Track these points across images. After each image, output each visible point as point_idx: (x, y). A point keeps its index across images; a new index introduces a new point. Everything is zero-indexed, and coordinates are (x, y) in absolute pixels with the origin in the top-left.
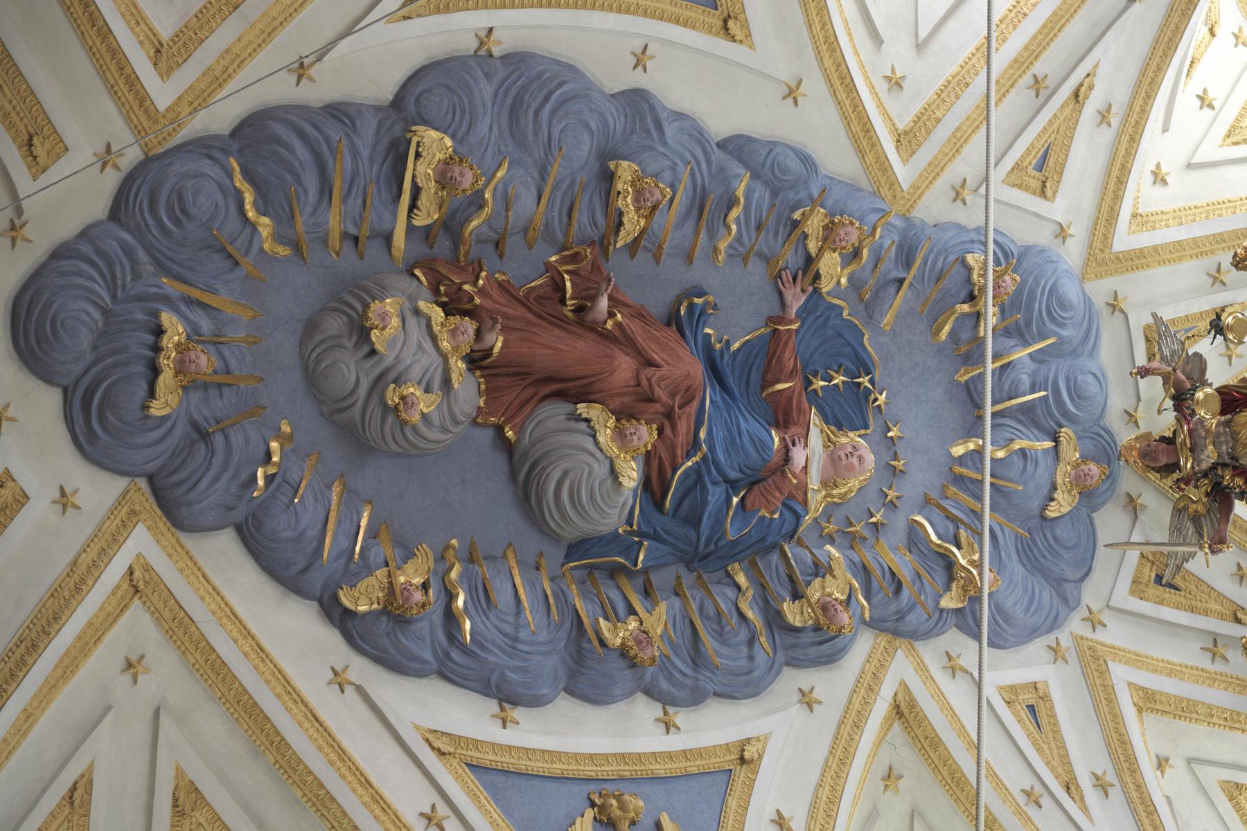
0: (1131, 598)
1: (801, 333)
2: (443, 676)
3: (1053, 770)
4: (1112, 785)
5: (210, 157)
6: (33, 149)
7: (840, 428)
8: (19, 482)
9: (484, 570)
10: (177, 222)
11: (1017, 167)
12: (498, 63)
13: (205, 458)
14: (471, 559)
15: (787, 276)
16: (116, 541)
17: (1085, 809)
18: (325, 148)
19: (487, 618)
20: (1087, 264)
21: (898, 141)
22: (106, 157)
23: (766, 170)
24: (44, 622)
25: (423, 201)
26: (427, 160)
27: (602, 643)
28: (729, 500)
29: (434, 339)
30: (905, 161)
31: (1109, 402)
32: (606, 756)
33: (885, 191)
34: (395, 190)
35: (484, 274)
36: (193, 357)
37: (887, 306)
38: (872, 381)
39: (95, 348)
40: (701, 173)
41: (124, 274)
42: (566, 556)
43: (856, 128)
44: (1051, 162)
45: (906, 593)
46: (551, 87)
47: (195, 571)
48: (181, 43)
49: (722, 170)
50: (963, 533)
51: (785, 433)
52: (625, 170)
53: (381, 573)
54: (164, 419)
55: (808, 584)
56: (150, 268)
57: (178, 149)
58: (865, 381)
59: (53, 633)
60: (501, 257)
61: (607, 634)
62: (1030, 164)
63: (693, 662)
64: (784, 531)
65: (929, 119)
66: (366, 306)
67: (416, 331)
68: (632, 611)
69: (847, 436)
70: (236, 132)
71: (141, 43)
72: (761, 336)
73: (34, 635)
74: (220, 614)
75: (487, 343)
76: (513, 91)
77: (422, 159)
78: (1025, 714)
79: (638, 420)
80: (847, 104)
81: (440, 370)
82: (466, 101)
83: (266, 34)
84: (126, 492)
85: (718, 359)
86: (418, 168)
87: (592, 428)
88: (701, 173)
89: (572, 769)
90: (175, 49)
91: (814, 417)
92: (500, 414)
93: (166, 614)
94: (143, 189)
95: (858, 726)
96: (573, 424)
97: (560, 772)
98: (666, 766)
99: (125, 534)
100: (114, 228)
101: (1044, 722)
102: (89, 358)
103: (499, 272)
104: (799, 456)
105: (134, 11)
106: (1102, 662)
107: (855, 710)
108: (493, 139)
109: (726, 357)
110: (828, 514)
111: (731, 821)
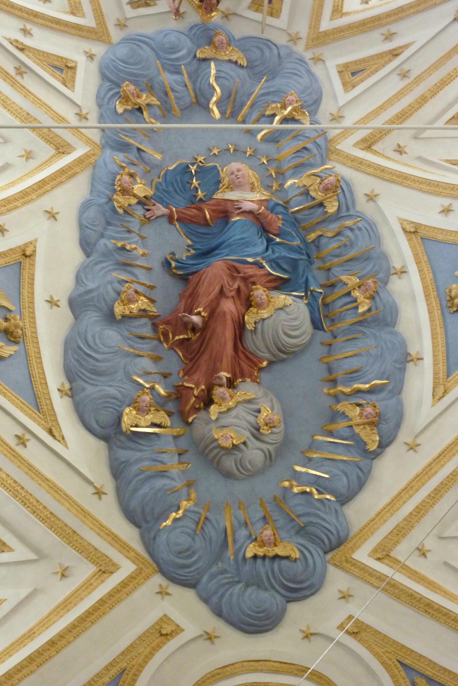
0: (281, 18)
1: (176, 206)
2: (400, 392)
3: (387, 63)
4: (389, 30)
5: (154, 538)
6: (169, 633)
7: (219, 182)
8: (342, 621)
9: (339, 374)
10: (194, 553)
11: (64, 84)
12: (73, 384)
13: (314, 526)
14: (334, 382)
15: (148, 214)
16: (364, 568)
17: (407, 46)
18: (141, 477)
19: (367, 371)
20: (104, 41)
21: (63, 153)
22: (162, 593)
23: (97, 229)
24: (414, 601)
25: (157, 421)
26: (138, 420)
27: (369, 310)
28: (279, 244)
29: (229, 410)
30: (74, 149)
31: (175, 29)
32: (428, 305)
33: (92, 160)
34: (153, 436)
35: (186, 384)
36: (267, 538)
37: (151, 157)
38: (193, 164)
39: (266, 589)
40: (107, 266)
41: (226, 578)
42: (320, 330)
43: (63, 178)
44: (57, 64)
45: (309, 146)
46: (83, 355)
47: (370, 526)
48: (98, 560)
49: (104, 255)
50: (267, 113)
51: (232, 213)
52: (119, 309)
53: (357, 430)
54: (300, 550)
55: (313, 199)
56: (220, 564)
57: (152, 555)
58: (193, 169)
59: (420, 596)
60: (171, 374)
61: (366, 308)
62: (60, 76)
63: (366, 260)
64: (285, 212)
65: (49, 136)
66: (219, 446)
67: (228, 420)
68: (349, 294)
69: (224, 178)
70: (137, 525)
71: (102, 582)
72: (181, 227)
73: (422, 606)
74: (392, 511)
75: (225, 380)
76: (89, 375)
77: (138, 424)
78: (357, 78)
79: (251, 296)
80: (52, 184)
81: (246, 405)
82: (100, 401)
83: (86, 514)
84: (335, 565)
85: (200, 251)
86: (143, 425)
87: (260, 321)
88: (107, 266)
89: (438, 322)
90: (101, 563)
91: (219, 196)
92: (252, 370)
93: (396, 539)
94: (178, 572)
95: (383, 170)
96: (259, 331)
97: (442, 329)
98: (427, 273)
99: (360, 564)
100: (200, 587)
101: (360, 67)
102: (273, 592)
103: (178, 375)
104: (248, 206)
105: (85, 587)
106: (319, 35)
107: (374, 171)
108: (115, 384)
109: (198, 246)
110: (268, 188)
111: (451, 238)
